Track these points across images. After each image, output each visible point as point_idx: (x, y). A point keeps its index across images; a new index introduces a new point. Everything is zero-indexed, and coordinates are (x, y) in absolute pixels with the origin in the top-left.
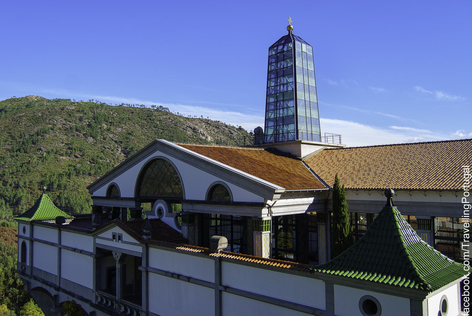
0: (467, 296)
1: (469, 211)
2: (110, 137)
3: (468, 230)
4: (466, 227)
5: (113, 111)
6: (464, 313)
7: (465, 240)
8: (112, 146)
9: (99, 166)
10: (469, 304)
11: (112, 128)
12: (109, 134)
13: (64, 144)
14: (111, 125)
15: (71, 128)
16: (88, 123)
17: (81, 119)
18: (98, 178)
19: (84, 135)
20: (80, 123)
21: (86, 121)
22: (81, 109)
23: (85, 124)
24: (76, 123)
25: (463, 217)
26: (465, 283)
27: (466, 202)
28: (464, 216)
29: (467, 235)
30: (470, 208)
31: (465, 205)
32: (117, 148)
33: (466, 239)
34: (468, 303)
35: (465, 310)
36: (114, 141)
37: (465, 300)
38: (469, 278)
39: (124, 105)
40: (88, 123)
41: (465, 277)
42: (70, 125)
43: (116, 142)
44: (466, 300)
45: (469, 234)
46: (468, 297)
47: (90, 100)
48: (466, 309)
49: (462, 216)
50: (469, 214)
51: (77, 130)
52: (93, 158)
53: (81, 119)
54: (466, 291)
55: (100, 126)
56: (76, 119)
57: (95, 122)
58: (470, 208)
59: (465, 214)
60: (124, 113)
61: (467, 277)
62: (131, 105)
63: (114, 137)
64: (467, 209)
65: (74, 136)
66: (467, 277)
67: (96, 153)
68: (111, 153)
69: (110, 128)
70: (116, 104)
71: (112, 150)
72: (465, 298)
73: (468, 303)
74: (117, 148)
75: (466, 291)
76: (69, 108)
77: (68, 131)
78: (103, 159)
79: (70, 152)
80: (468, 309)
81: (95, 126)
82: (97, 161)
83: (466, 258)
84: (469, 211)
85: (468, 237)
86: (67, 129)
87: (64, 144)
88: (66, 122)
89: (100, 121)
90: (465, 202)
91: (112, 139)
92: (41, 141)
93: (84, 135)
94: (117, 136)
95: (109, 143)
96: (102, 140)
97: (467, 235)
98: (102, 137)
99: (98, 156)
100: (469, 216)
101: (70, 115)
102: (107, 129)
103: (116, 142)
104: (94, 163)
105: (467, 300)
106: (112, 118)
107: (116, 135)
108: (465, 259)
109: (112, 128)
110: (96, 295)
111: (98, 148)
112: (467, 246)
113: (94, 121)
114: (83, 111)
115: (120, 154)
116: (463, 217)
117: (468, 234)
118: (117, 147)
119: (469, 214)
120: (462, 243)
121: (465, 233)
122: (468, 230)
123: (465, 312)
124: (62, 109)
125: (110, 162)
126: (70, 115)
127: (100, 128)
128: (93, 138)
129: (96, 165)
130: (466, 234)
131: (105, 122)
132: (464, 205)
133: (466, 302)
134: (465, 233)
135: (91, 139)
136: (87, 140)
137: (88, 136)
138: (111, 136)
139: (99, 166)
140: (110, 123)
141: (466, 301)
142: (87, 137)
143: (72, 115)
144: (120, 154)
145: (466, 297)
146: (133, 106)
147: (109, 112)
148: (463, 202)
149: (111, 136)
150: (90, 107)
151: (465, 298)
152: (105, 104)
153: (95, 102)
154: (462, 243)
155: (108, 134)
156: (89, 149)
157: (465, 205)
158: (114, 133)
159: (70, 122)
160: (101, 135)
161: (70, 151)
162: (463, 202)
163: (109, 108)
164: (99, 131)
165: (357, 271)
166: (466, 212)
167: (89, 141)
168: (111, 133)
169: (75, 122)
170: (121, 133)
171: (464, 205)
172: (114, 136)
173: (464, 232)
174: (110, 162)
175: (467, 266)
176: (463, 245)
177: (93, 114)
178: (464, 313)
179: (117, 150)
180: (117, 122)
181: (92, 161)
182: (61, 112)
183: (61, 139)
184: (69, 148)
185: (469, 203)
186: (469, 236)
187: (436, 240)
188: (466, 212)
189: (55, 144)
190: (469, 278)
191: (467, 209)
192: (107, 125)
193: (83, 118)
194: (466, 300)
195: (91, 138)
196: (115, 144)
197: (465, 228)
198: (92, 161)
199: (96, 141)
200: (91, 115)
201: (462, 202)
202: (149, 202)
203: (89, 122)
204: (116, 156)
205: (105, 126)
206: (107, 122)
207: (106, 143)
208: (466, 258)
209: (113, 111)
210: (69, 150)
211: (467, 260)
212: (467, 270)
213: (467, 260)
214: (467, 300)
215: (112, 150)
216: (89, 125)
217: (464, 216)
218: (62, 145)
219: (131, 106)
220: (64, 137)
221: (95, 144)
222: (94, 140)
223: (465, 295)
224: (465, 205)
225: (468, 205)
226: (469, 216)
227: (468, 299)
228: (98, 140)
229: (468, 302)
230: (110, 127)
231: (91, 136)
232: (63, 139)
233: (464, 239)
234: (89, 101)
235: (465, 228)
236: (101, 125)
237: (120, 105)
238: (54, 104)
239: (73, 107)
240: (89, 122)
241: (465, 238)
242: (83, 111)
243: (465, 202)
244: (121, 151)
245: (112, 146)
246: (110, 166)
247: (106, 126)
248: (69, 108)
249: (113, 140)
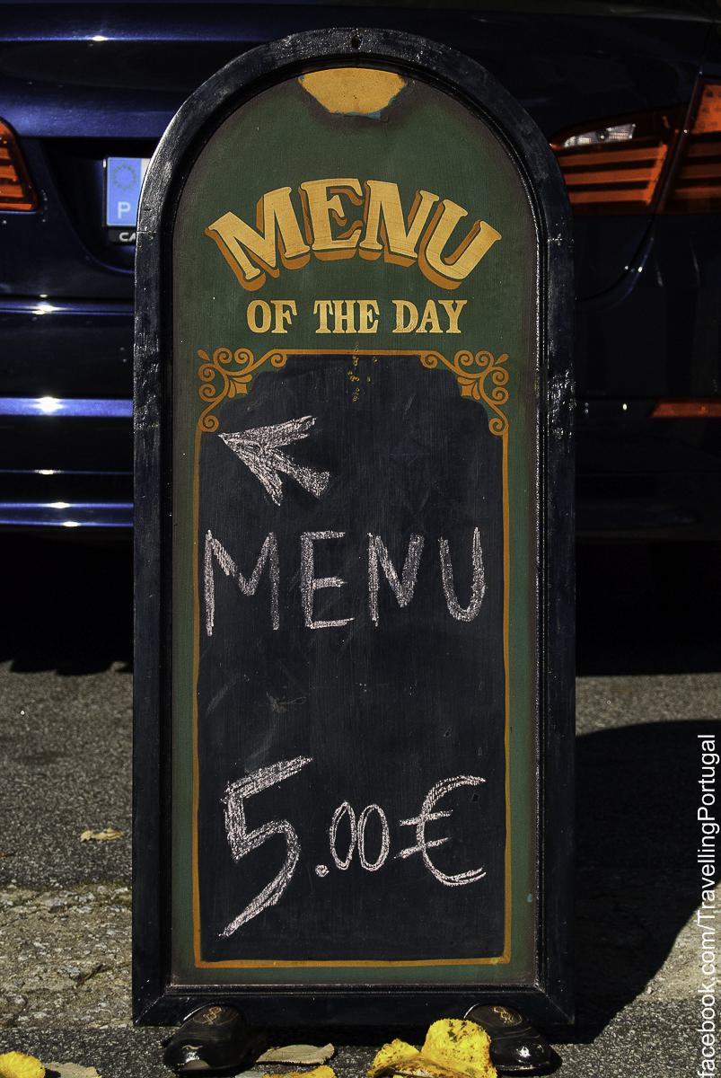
0: (708, 1033)
1: (713, 838)
4: (708, 874)
7: (706, 788)
10: (459, 879)
26: (283, 836)
27: (707, 818)
30: (717, 763)
31: (704, 825)
44: (706, 872)
54: (474, 357)
58: (717, 763)
59: (704, 845)
75: (707, 835)
80: (712, 742)
83: (710, 772)
84: (713, 838)
90: (704, 817)
100: (713, 861)
141: (707, 1044)
148: (701, 816)
157: (704, 825)
162: (701, 816)
165: (462, 398)
166: (706, 841)
187: (713, 736)
188: (706, 841)
191: (706, 952)
194: (706, 872)
201: (699, 819)
211: (711, 793)
213: (711, 793)
214: (710, 872)
225: (712, 825)
226: (713, 861)
243: (704, 817)
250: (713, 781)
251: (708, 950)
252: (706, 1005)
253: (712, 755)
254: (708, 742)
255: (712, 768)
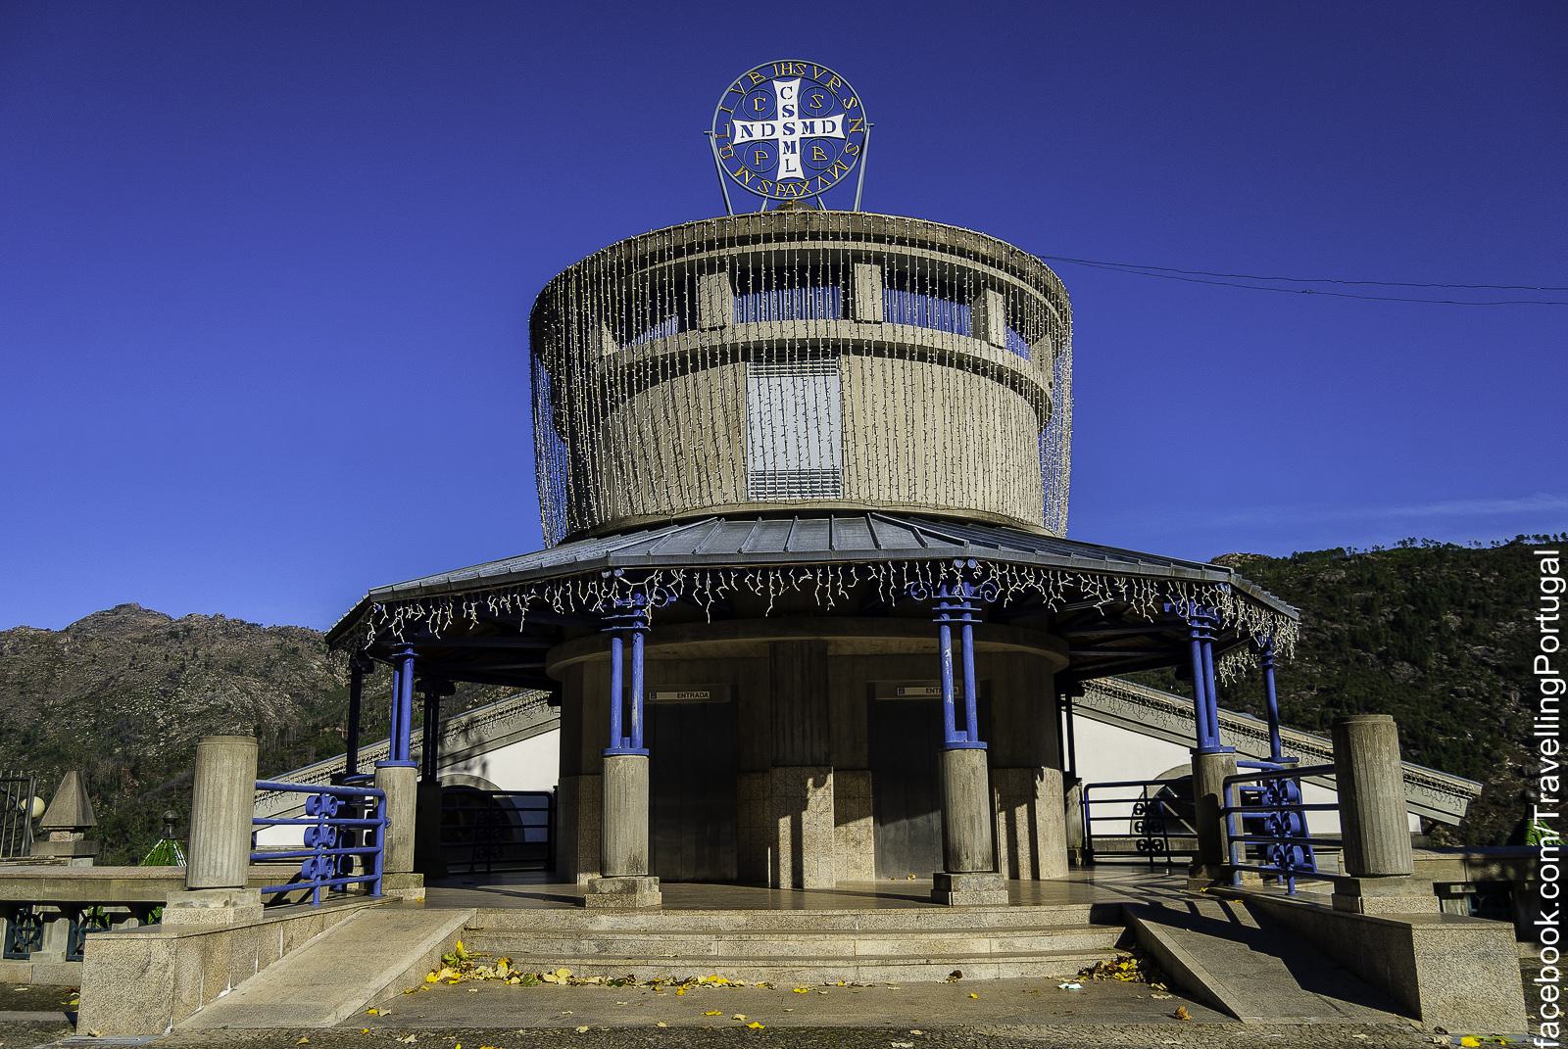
1: (1557, 700)
2: (1475, 657)
3: (1556, 765)
4: (1549, 753)
5: (1484, 566)
6: (1542, 1040)
8: (1483, 685)
9: (1433, 756)
11: (1481, 624)
12: (1468, 645)
13: (1315, 692)
14: (1474, 616)
15: (1336, 640)
16: (1392, 617)
17: (1367, 608)
19: (1379, 655)
20: (1367, 619)
21: (1386, 610)
22: (1367, 576)
23: (1381, 620)
24: (1351, 622)
25: (1539, 718)
26: (1544, 938)
27: (1547, 671)
28: (1543, 719)
30: (1562, 692)
31: (1544, 681)
32: (1503, 692)
34: (1554, 1005)
36: (1492, 668)
37: (1546, 995)
38: (1557, 923)
39: (1526, 542)
40: (1392, 617)
41: (1545, 920)
42: (1332, 628)
43: (1498, 670)
45: (1557, 777)
47: (1404, 543)
48: (1549, 1024)
49: (1536, 719)
50: (1557, 711)
51: (1355, 644)
52: (1414, 732)
53: (1367, 608)
55: (1434, 623)
56: (1351, 609)
57: (1417, 612)
58: (1562, 692)
59: (1544, 711)
60: (1525, 567)
61: (1552, 919)
62: (1555, 536)
63: (1489, 654)
65: (1347, 662)
66: (1552, 919)
67: (1426, 713)
68: (1483, 711)
69: (1472, 624)
70: (1493, 542)
71: (1485, 697)
72: (1546, 991)
73: (1554, 1005)
74: (1503, 692)
75: (1547, 965)
76: (1327, 577)
77: (1327, 649)
78: (1449, 733)
79: (1333, 716)
81: (1418, 623)
82: (1426, 739)
83: (1547, 854)
84: (1557, 700)
85: (1554, 786)
86: (1324, 642)
87: (1315, 692)
88: (1320, 622)
89: (1435, 605)
91: (1485, 661)
92: (1246, 688)
93: (1379, 655)
94: (1500, 650)
95: (1473, 676)
96: (1445, 667)
98: (1445, 657)
99: (1429, 724)
101: (1331, 598)
102: (1462, 630)
103: (1498, 670)
104: (1416, 747)
106: (1480, 589)
107: (1496, 648)
109: (1481, 624)
111: (1433, 695)
112: (645, 661)
113: (1412, 608)
114: (1372, 581)
115: (1518, 711)
116: (1539, 718)
118: (1504, 688)
119: (1557, 711)
120: (1536, 807)
122: (1556, 765)
124: (1307, 584)
125: (1476, 742)
126: (1331, 598)
127: (1436, 629)
128: (1413, 663)
129: (1425, 754)
130: (1549, 778)
131: (1453, 606)
132: (1542, 680)
133: (1550, 1004)
135: (1405, 669)
136: (1392, 673)
137: (1396, 660)
138: (1479, 650)
139: (1433, 756)
140: (1473, 607)
141: (1549, 1000)
142: (1392, 664)
143: (1338, 597)
144: (1518, 711)
146: (1561, 540)
147: (1466, 571)
149: (1479, 650)
150: (1401, 566)
152: (1453, 546)
153: (1419, 545)
154: (1536, 807)
155: (1466, 648)
156: (1400, 700)
157: (1544, 681)
158: (1487, 641)
159: (1332, 620)
160: (1442, 650)
161: (1334, 712)
163: (1468, 559)
164: (1430, 639)
166: (1548, 705)
167: (1398, 674)
168: (1475, 642)
169: (1348, 619)
170: (1514, 639)
171: (1542, 680)
172: (1492, 651)
173: (1543, 771)
174: (1476, 742)
175: (1551, 883)
176: (1536, 815)
177: (1409, 585)
178: (1542, 1040)
179: (1505, 696)
180: (1497, 603)
181: (1409, 741)
182: (1302, 592)
183: (1305, 675)
184: (1331, 703)
185: (1557, 672)
186: (1557, 782)
188: (1548, 705)
189: (1289, 694)
190: (1557, 923)
192: (1460, 615)
193: (1376, 604)
195: (1405, 664)
196: (1495, 677)
197: (1547, 757)
198: (1409, 741)
199: (1425, 673)
200: (1401, 589)
201: (1536, 672)
203: (1395, 613)
204: (1502, 720)
205: (1453, 620)
206: (1460, 604)
207: (1461, 676)
208: (1547, 854)
209: (1484, 566)
210: (1331, 709)
214: (1552, 996)
215: (1485, 700)
216: (1397, 624)
217: (1543, 719)
218: (1307, 695)
219: (1552, 539)
220: (1315, 671)
221: (1420, 685)
222: (1416, 672)
223: (1544, 979)
224: (1544, 681)
225: (1555, 681)
227: (1554, 993)
228: (1430, 669)
229: (1554, 1002)
230: (1472, 620)
231: (1403, 660)
232: (1314, 677)
234: (1401, 546)
235: (1547, 757)
236: (1437, 618)
237: (1512, 544)
238: (1285, 571)
239: (1339, 574)
240: (1395, 613)
241: (1545, 789)
242: (1372, 581)
244: (1521, 700)
245: (1483, 685)
246: (1475, 754)
247: (1457, 620)
248: (1327, 577)
249: (1485, 664)
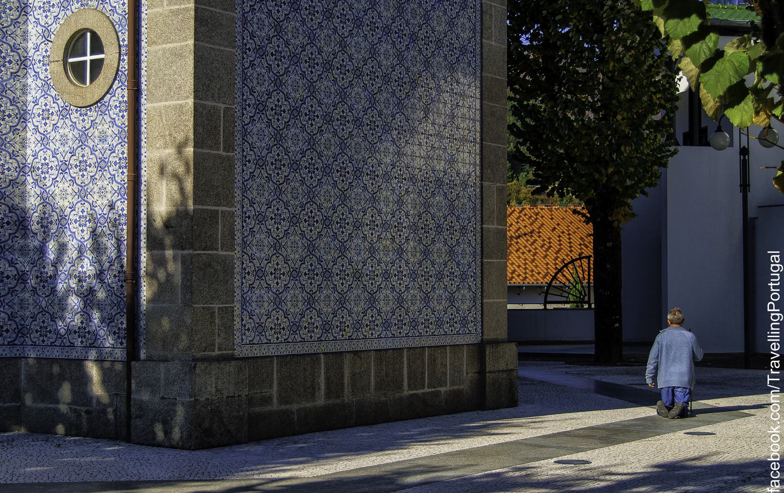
0: (776, 461)
1: (779, 324)
4: (775, 350)
18: (746, 35)
27: (774, 310)
28: (772, 333)
29: (777, 363)
31: (772, 314)
33: (775, 369)
35: (773, 483)
37: (773, 467)
46: (778, 344)
48: (775, 481)
50: (779, 329)
59: (772, 329)
64: (774, 435)
72: (773, 345)
84: (779, 324)
85: (777, 365)
97: (777, 363)
105: (777, 348)
108: (772, 290)
110: (747, 8)
117: (778, 362)
119: (779, 329)
121: (774, 360)
122: (778, 355)
123: (772, 486)
130: (775, 362)
133: (775, 471)
134: (774, 360)
141: (775, 469)
145: (775, 463)
151: (773, 345)
157: (772, 314)
166: (774, 326)
173: (772, 358)
176: (769, 379)
185: (779, 310)
188: (774, 326)
191: (774, 435)
201: (769, 310)
202: (745, 350)
212: (777, 419)
214: (777, 348)
217: (772, 333)
227: (777, 347)
229: (778, 470)
233: (771, 370)
250: (779, 283)
251: (774, 403)
252: (778, 435)
253: (778, 265)
254: (775, 256)
255: (778, 275)
